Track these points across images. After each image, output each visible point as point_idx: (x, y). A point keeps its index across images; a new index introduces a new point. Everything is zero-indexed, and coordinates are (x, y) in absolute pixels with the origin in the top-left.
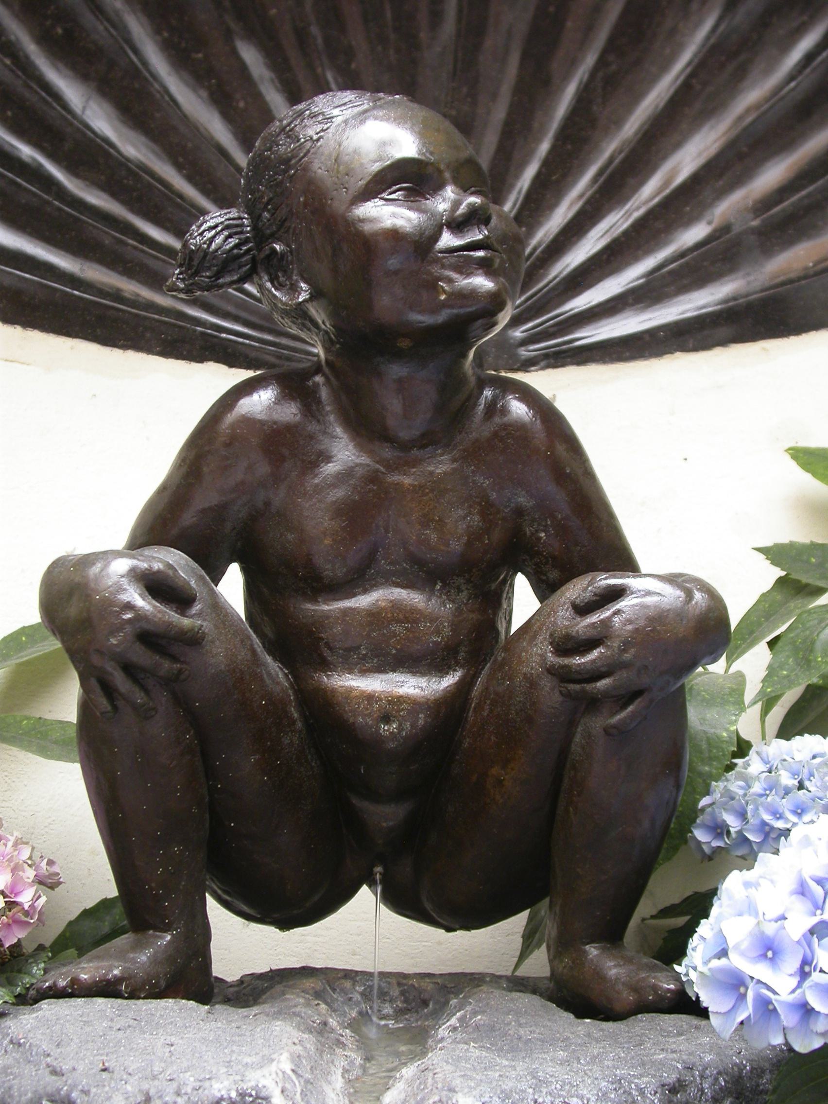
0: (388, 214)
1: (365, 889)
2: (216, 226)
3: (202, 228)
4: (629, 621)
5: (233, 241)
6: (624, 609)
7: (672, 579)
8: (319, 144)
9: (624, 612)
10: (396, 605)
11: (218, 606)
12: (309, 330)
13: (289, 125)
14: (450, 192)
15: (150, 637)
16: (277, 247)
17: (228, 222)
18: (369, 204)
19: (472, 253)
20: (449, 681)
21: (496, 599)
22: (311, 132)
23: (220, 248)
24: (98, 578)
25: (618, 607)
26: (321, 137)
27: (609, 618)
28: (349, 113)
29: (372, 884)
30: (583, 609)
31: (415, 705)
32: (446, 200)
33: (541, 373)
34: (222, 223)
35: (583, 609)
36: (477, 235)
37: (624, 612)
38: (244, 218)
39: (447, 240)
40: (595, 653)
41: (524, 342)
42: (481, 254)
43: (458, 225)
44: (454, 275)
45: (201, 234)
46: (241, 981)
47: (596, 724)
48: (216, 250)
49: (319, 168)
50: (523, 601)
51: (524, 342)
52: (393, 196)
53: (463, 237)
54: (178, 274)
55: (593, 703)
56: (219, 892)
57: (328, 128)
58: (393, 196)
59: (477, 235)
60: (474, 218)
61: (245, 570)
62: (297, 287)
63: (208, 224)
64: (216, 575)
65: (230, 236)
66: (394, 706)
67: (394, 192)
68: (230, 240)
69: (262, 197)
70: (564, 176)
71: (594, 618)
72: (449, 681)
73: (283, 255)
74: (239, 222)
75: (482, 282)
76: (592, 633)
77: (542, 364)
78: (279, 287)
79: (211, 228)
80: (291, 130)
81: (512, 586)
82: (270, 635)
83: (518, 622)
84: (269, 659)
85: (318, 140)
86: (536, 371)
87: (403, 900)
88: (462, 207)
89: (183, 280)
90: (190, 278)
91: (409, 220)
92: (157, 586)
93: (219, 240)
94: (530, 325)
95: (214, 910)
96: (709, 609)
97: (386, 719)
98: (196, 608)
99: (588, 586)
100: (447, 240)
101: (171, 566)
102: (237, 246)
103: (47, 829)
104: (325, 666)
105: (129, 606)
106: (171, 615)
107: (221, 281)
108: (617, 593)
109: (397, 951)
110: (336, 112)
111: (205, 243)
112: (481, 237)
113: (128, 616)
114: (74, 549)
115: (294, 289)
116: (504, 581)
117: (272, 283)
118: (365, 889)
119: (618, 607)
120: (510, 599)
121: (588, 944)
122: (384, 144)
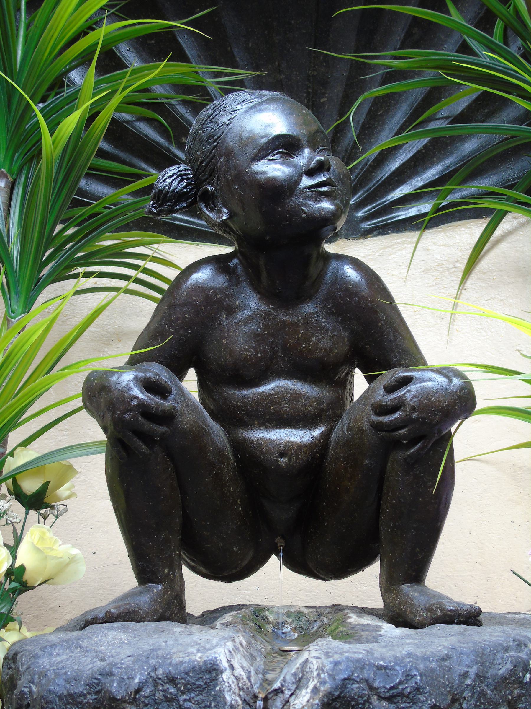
0: (273, 169)
1: (274, 558)
2: (173, 176)
3: (165, 177)
4: (415, 396)
5: (184, 184)
6: (412, 389)
7: (441, 371)
8: (230, 127)
9: (412, 391)
10: (286, 391)
11: (182, 393)
12: (229, 233)
13: (212, 114)
14: (306, 152)
15: (145, 411)
16: (209, 188)
17: (179, 173)
18: (261, 163)
19: (319, 189)
20: (317, 432)
21: (344, 384)
22: (225, 119)
23: (176, 189)
24: (117, 383)
25: (409, 388)
26: (231, 123)
27: (403, 395)
28: (246, 106)
29: (277, 555)
30: (390, 389)
31: (300, 446)
32: (305, 158)
33: (375, 238)
34: (176, 173)
35: (390, 389)
36: (322, 178)
37: (412, 391)
38: (189, 170)
39: (306, 182)
40: (396, 415)
41: (365, 219)
42: (325, 189)
43: (311, 173)
44: (311, 203)
45: (165, 180)
46: (203, 615)
47: (401, 455)
48: (174, 190)
49: (231, 142)
50: (359, 384)
51: (365, 219)
52: (274, 158)
53: (314, 179)
54: (152, 204)
55: (397, 444)
56: (189, 561)
57: (235, 117)
58: (274, 158)
59: (322, 178)
60: (321, 167)
61: (198, 373)
62: (221, 211)
63: (169, 175)
64: (181, 374)
65: (182, 181)
66: (286, 450)
67: (277, 154)
68: (181, 183)
69: (198, 159)
70: (387, 112)
71: (396, 395)
72: (317, 432)
73: (213, 193)
74: (187, 172)
75: (326, 205)
76: (395, 403)
77: (375, 233)
78: (212, 210)
79: (170, 177)
80: (213, 118)
81: (353, 376)
82: (212, 407)
83: (357, 396)
84: (214, 423)
85: (229, 125)
86: (372, 237)
87: (298, 563)
88: (313, 162)
89: (155, 208)
90: (159, 207)
91: (283, 172)
92: (151, 386)
93: (175, 184)
94: (366, 209)
95: (185, 571)
96: (462, 389)
97: (282, 454)
98: (172, 397)
99: (392, 377)
100: (306, 182)
101: (157, 374)
102: (185, 187)
103: (81, 531)
104: (247, 425)
105: (136, 398)
106: (158, 400)
107: (177, 207)
108: (407, 381)
109: (296, 598)
110: (239, 107)
111: (167, 186)
112: (325, 179)
113: (134, 403)
114: (476, 603)
115: (220, 211)
116: (347, 374)
117: (207, 209)
118: (274, 558)
119: (409, 388)
120: (352, 383)
121: (403, 584)
122: (267, 126)
